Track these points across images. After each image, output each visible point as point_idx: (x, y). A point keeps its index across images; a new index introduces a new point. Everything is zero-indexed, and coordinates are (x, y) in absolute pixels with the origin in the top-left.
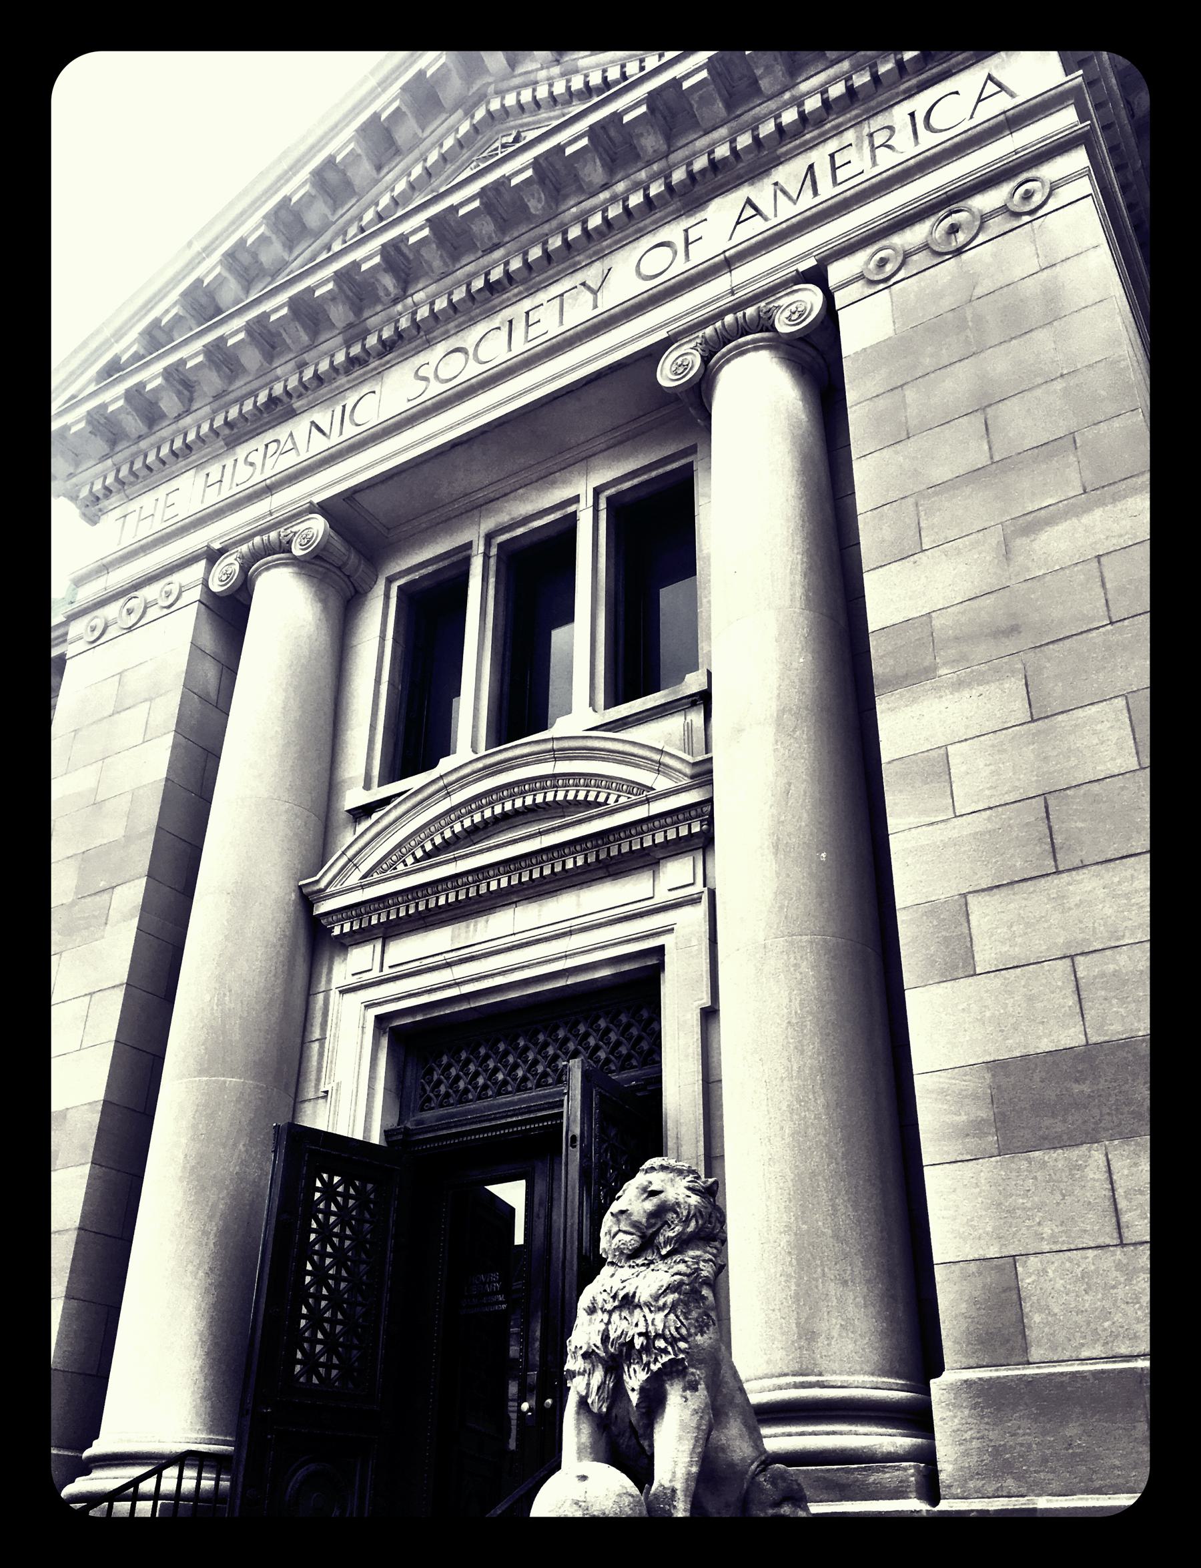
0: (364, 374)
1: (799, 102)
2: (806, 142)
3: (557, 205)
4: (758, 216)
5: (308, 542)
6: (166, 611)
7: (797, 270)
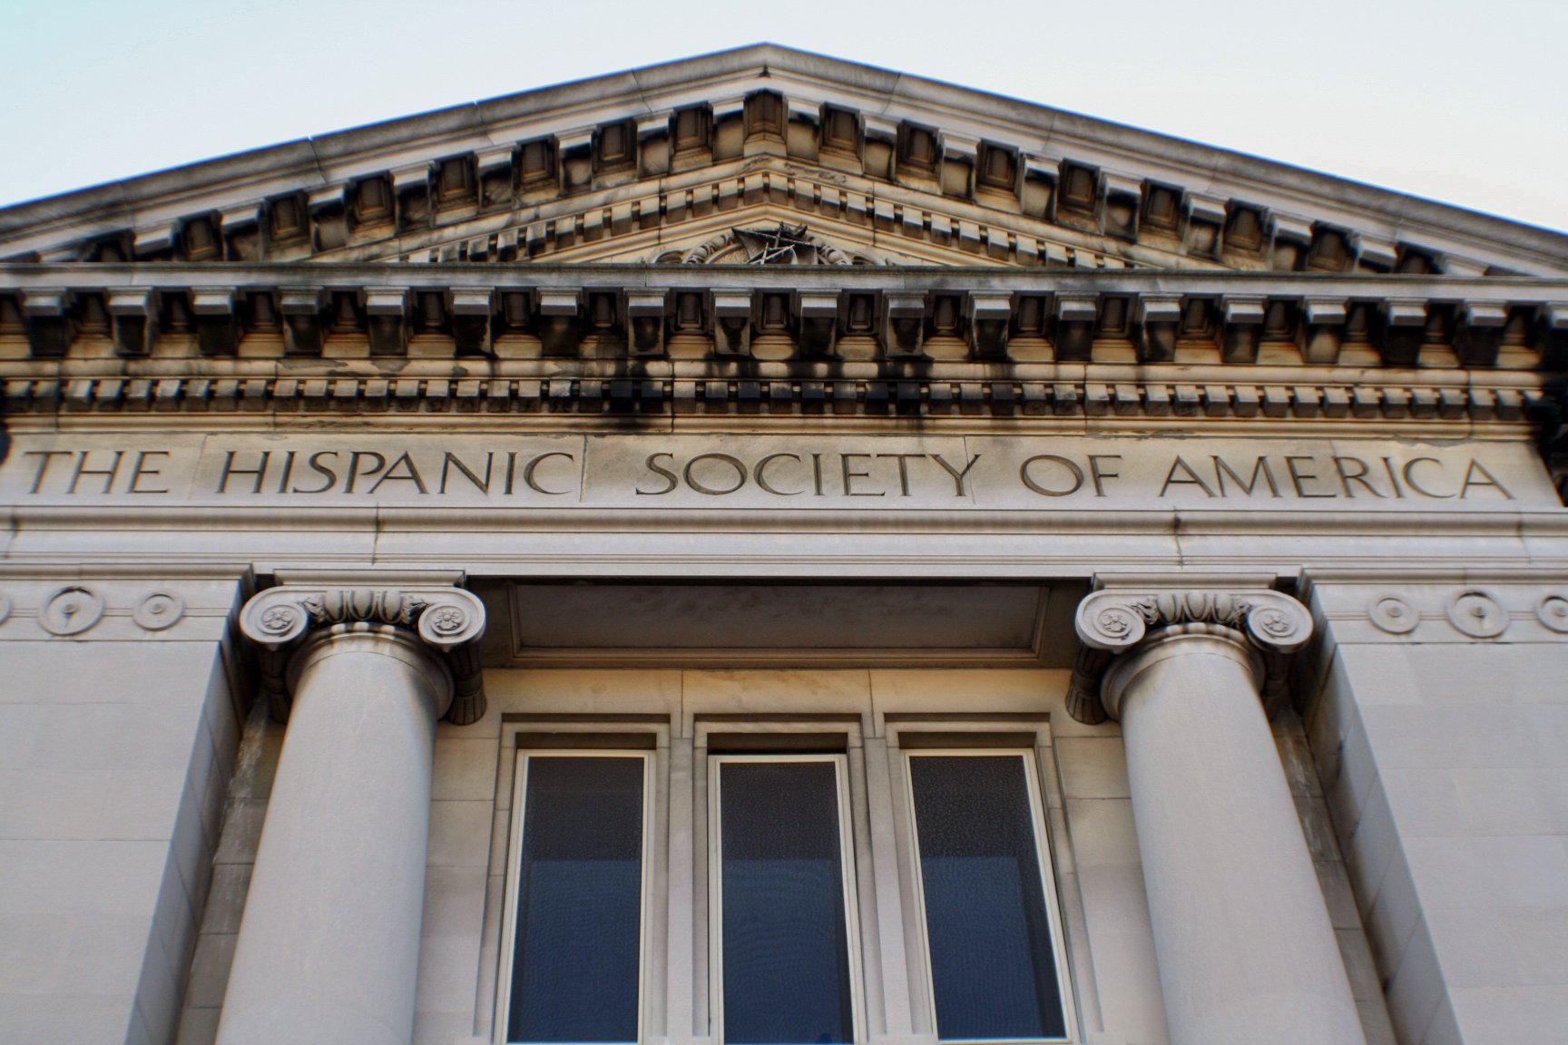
0: (803, 427)
1: (392, 377)
2: (824, 427)
3: (926, 339)
4: (1299, 474)
5: (284, 626)
6: (140, 634)
7: (464, 571)
